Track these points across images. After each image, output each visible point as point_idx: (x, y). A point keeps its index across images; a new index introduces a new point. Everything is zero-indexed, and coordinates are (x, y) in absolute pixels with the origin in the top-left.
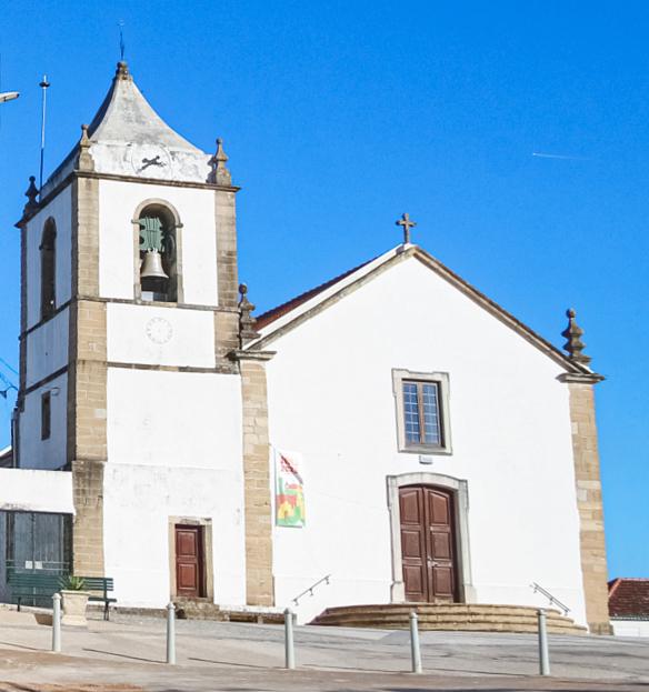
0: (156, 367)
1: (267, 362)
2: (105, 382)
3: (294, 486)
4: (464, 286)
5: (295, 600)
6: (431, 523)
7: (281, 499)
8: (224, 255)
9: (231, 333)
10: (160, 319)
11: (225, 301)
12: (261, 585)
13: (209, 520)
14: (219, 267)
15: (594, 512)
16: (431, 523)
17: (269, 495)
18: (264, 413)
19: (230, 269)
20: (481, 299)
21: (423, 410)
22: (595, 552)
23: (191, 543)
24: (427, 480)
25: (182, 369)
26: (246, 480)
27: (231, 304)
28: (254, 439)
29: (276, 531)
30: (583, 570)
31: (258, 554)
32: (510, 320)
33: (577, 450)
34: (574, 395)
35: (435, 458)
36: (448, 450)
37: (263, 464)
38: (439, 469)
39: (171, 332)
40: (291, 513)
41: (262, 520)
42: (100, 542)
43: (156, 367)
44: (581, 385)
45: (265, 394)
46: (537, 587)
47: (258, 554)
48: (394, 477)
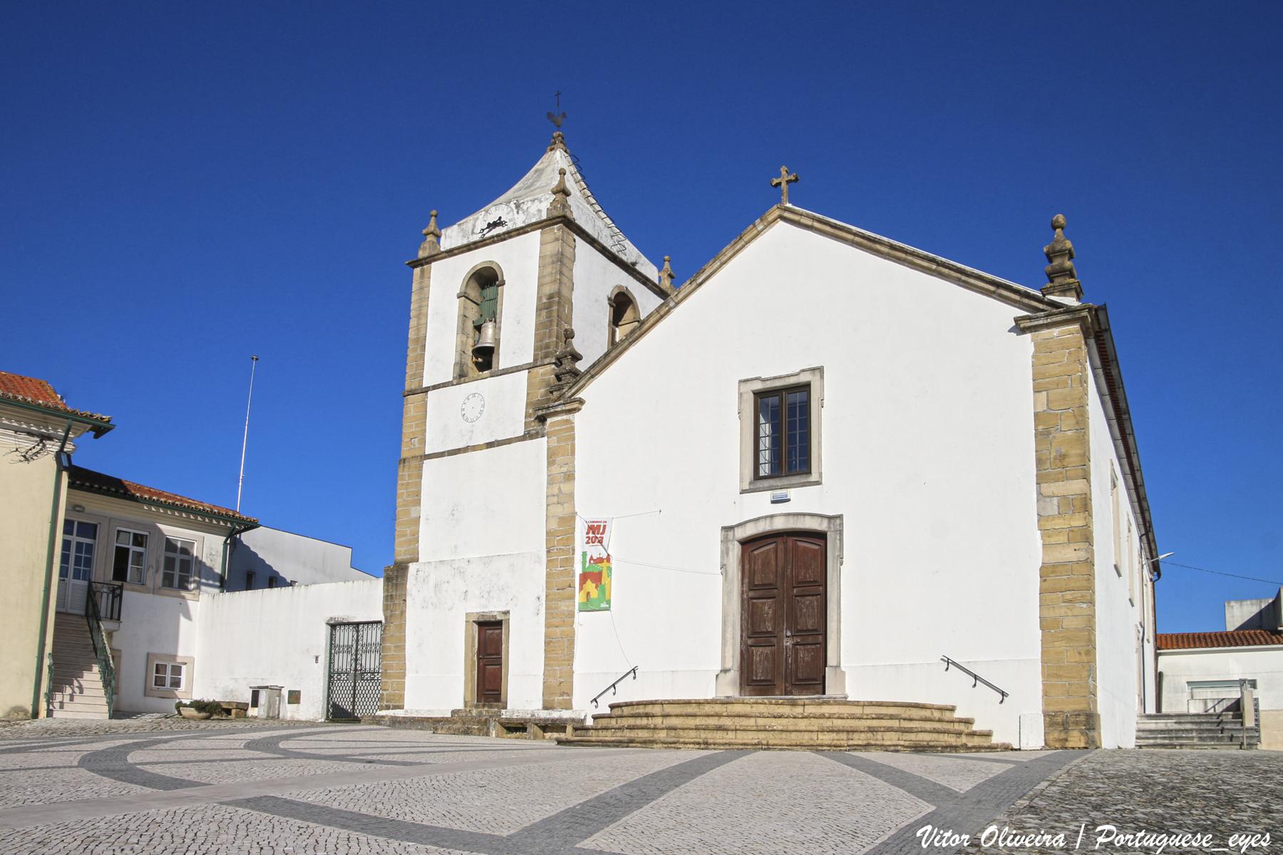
0: (466, 450)
1: (577, 415)
2: (420, 477)
3: (600, 560)
4: (850, 237)
5: (595, 700)
6: (785, 590)
7: (585, 577)
8: (545, 300)
9: (543, 390)
10: (474, 395)
11: (541, 354)
12: (558, 687)
13: (507, 613)
14: (538, 315)
15: (1071, 530)
16: (785, 590)
17: (573, 576)
18: (570, 477)
19: (549, 316)
20: (878, 247)
21: (784, 425)
22: (1068, 595)
23: (489, 637)
24: (779, 524)
25: (490, 445)
26: (548, 561)
27: (546, 356)
28: (560, 511)
29: (580, 617)
30: (1042, 628)
31: (559, 648)
32: (925, 264)
33: (1042, 436)
34: (1041, 349)
35: (792, 493)
36: (814, 477)
37: (568, 539)
38: (801, 504)
39: (483, 406)
40: (595, 594)
41: (563, 606)
42: (403, 648)
43: (466, 450)
44: (1055, 332)
45: (573, 453)
46: (948, 662)
47: (559, 648)
48: (732, 528)
